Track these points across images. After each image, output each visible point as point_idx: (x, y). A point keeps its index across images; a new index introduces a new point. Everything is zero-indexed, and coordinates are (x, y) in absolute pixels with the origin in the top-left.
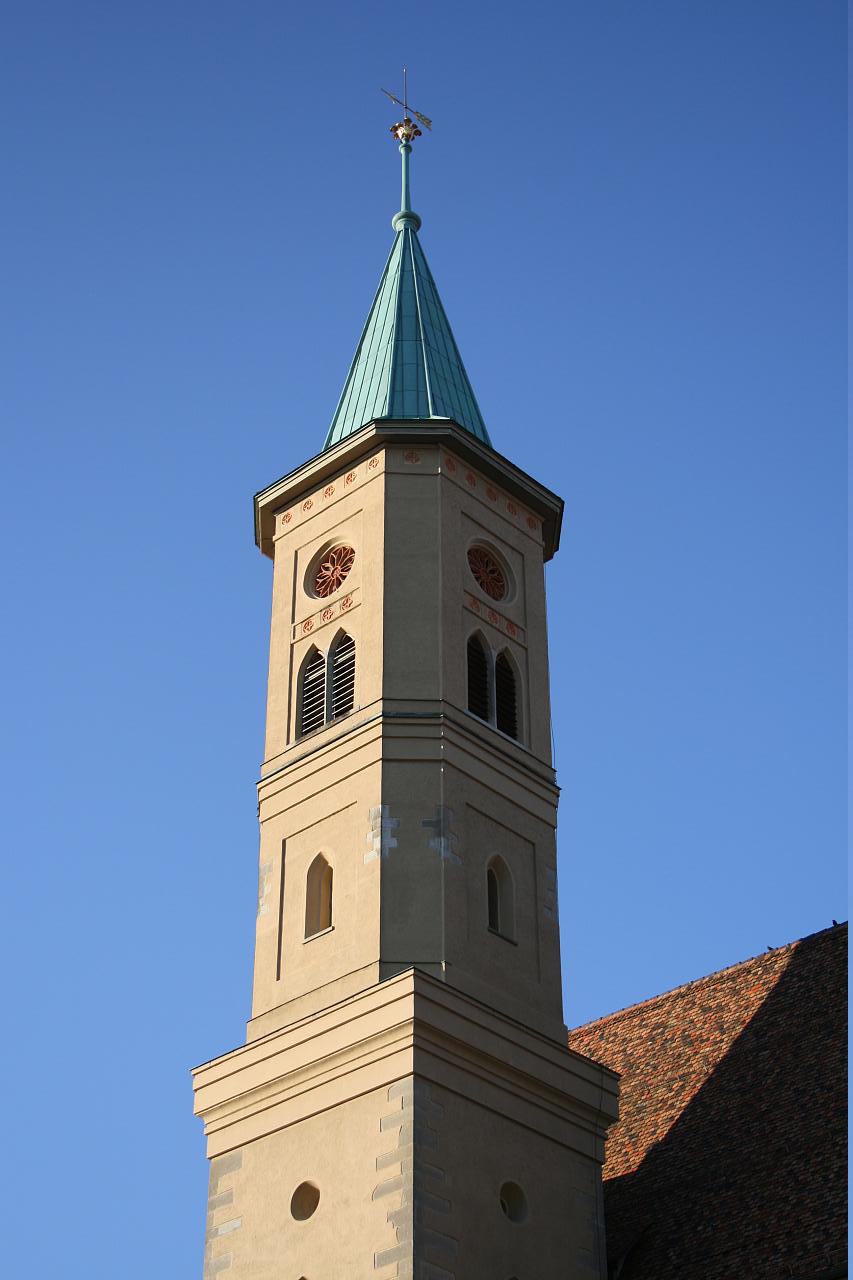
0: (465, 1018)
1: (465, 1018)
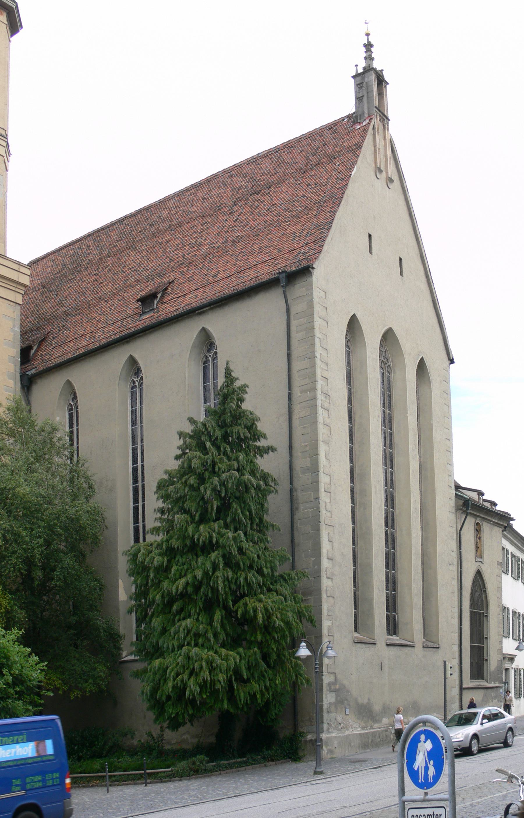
0: (289, 356)
1: (289, 356)
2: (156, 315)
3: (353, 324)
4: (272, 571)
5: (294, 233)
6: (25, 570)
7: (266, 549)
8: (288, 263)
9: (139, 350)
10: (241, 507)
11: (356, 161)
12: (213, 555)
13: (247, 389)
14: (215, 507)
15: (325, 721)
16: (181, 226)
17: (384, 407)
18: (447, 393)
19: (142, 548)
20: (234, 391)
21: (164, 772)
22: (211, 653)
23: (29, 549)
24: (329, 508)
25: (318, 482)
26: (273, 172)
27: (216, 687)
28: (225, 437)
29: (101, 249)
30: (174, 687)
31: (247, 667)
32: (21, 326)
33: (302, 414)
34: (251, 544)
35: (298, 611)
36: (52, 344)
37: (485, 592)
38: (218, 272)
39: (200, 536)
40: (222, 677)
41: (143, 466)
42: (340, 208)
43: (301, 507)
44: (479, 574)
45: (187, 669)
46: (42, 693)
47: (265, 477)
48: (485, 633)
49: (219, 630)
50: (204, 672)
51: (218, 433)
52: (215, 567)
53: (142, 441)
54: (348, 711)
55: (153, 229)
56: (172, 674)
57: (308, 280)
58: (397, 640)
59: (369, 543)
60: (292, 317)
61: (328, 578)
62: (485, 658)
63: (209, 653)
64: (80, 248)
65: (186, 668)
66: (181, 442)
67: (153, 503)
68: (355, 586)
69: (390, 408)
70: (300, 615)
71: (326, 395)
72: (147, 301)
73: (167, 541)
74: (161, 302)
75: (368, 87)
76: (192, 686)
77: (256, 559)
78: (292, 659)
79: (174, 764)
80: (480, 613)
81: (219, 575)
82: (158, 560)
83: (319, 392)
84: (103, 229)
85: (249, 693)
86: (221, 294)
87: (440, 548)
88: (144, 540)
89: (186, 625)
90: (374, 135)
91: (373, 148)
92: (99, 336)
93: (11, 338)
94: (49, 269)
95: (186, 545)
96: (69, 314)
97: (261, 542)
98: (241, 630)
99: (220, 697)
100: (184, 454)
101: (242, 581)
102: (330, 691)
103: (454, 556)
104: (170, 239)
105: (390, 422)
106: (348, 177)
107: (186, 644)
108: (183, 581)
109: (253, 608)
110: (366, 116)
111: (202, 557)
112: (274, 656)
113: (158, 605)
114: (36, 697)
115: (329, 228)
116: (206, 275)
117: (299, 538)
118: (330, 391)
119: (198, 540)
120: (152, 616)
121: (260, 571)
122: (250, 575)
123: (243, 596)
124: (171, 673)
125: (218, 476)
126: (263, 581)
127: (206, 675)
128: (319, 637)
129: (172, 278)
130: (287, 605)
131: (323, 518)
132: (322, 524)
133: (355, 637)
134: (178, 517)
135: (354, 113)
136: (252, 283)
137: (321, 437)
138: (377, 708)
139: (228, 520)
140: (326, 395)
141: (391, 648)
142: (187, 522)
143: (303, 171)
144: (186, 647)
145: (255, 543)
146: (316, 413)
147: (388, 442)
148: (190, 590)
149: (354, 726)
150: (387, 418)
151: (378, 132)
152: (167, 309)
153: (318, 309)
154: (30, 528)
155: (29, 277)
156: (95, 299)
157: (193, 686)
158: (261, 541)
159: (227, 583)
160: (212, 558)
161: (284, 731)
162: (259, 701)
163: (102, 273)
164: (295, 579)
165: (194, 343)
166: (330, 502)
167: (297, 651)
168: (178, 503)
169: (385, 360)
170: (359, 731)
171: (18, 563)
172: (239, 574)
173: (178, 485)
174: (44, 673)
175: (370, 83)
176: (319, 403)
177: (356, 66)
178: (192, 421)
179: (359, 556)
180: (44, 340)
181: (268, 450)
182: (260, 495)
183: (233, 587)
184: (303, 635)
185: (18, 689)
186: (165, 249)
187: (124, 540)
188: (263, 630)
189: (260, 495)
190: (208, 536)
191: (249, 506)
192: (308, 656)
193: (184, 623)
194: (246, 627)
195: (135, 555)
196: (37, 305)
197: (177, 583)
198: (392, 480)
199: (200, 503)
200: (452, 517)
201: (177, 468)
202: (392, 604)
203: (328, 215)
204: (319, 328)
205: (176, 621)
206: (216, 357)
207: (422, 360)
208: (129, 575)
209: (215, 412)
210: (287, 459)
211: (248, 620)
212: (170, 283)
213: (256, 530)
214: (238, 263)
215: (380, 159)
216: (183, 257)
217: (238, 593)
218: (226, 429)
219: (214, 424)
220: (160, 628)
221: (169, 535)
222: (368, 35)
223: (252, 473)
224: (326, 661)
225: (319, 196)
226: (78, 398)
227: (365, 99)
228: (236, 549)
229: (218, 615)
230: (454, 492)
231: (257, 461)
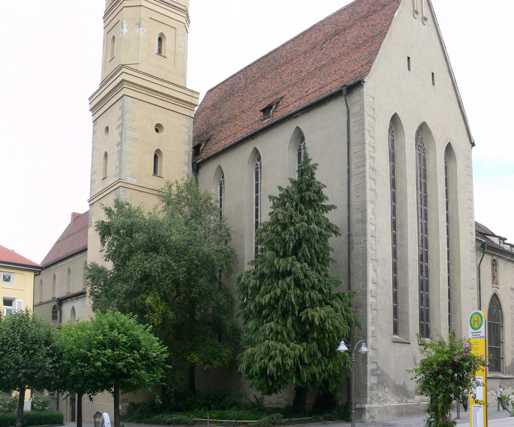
0: (349, 143)
1: (349, 143)
3: (395, 120)
4: (330, 291)
5: (356, 59)
7: (326, 275)
8: (349, 80)
10: (308, 246)
12: (288, 279)
13: (317, 166)
14: (291, 246)
15: (368, 395)
18: (469, 167)
21: (253, 422)
22: (284, 345)
24: (374, 248)
25: (366, 229)
28: (302, 200)
33: (356, 183)
34: (314, 272)
37: (501, 309)
38: (309, 89)
40: (290, 362)
42: (385, 40)
43: (355, 247)
44: (495, 296)
45: (268, 355)
48: (501, 338)
51: (296, 197)
57: (361, 90)
59: (406, 272)
60: (351, 117)
61: (372, 296)
62: (501, 357)
63: (283, 345)
64: (235, 80)
66: (271, 204)
69: (425, 178)
71: (373, 169)
72: (266, 111)
74: (275, 111)
79: (260, 419)
80: (497, 324)
82: (253, 282)
83: (367, 167)
84: (249, 66)
85: (310, 373)
87: (463, 277)
93: (187, 139)
98: (304, 331)
103: (475, 282)
104: (285, 70)
105: (425, 188)
109: (312, 315)
117: (353, 269)
118: (376, 167)
119: (279, 268)
121: (321, 291)
122: (312, 294)
127: (279, 359)
129: (283, 95)
132: (369, 259)
137: (368, 198)
140: (373, 169)
148: (272, 302)
149: (392, 400)
152: (277, 115)
159: (296, 297)
161: (342, 402)
162: (318, 379)
170: (396, 404)
176: (367, 175)
178: (280, 188)
183: (301, 301)
188: (320, 331)
193: (268, 325)
196: (208, 118)
197: (264, 297)
200: (473, 255)
203: (377, 45)
204: (368, 123)
215: (417, 3)
218: (305, 193)
220: (254, 328)
223: (318, 224)
229: (290, 321)
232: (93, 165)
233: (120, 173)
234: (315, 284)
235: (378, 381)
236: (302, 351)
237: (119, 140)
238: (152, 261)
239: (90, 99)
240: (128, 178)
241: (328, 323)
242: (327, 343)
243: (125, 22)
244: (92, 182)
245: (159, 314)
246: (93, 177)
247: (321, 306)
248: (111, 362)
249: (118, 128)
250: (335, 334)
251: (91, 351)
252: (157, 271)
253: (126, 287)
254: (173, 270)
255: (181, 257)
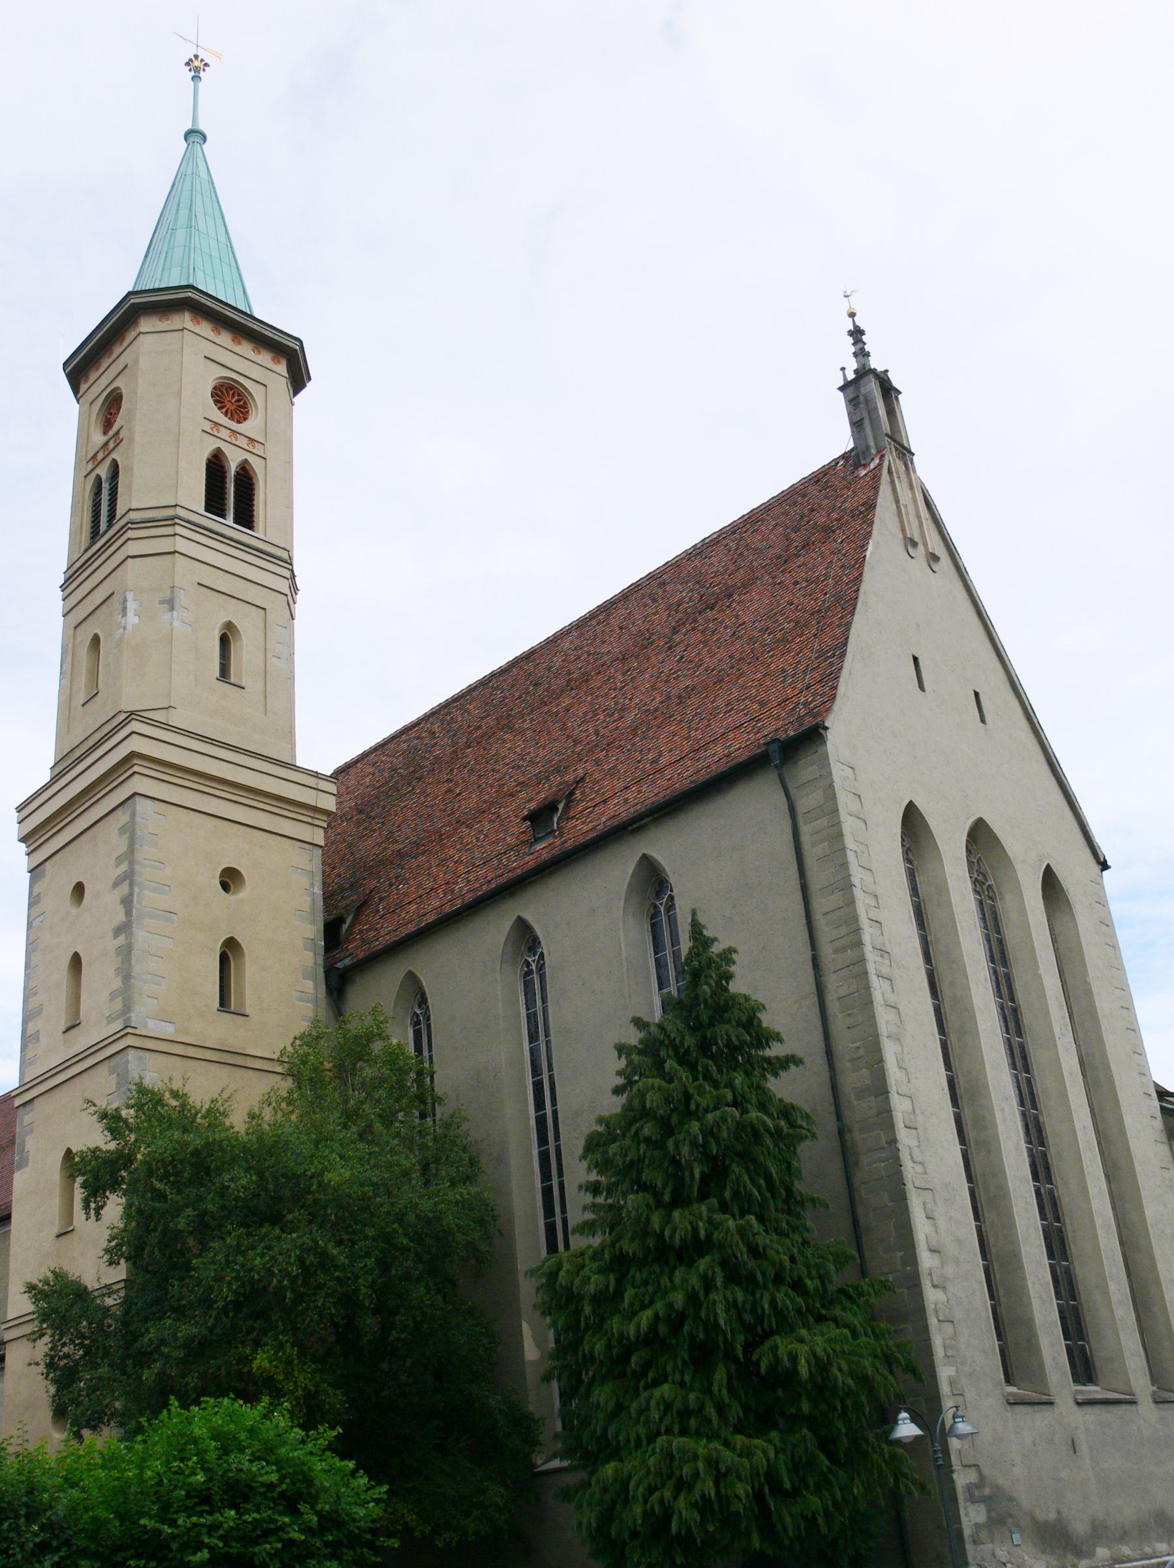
0: (804, 888)
1: (804, 888)
2: (558, 842)
3: (913, 823)
4: (823, 1283)
5: (784, 670)
6: (343, 1318)
7: (805, 1243)
9: (535, 908)
10: (748, 1170)
11: (870, 532)
12: (703, 1264)
15: (970, 1560)
16: (587, 680)
17: (993, 962)
18: (1106, 923)
19: (565, 1260)
20: (710, 961)
22: (715, 1444)
23: (349, 1278)
26: (732, 567)
27: (732, 1509)
28: (704, 1046)
29: (455, 735)
30: (645, 1514)
31: (790, 1465)
32: (324, 883)
33: (843, 992)
34: (775, 1237)
35: (885, 1355)
36: (378, 911)
39: (674, 1229)
40: (741, 1489)
41: (555, 1113)
42: (856, 617)
43: (865, 1160)
45: (669, 1477)
46: (378, 1543)
47: (787, 1112)
49: (727, 1400)
50: (704, 1481)
51: (690, 1041)
52: (708, 1284)
53: (550, 1068)
54: (1017, 1538)
55: (540, 690)
56: (641, 1489)
57: (820, 750)
58: (1096, 1391)
61: (935, 1286)
64: (418, 738)
65: (665, 1477)
67: (577, 1171)
68: (992, 1297)
70: (889, 1360)
71: (883, 952)
72: (540, 818)
73: (613, 1244)
74: (566, 816)
75: (868, 401)
76: (684, 1513)
77: (787, 1263)
78: (884, 1446)
81: (716, 1298)
82: (595, 1283)
83: (868, 949)
86: (668, 791)
88: (567, 1246)
89: (662, 1396)
90: (892, 483)
91: (894, 506)
92: (461, 889)
93: (307, 907)
94: (367, 779)
95: (648, 1249)
96: (407, 855)
97: (793, 1232)
98: (769, 1398)
99: (743, 1526)
100: (630, 1083)
101: (766, 1306)
102: (973, 1500)
104: (571, 706)
105: (1010, 988)
106: (860, 562)
107: (663, 1429)
108: (649, 1313)
109: (790, 1354)
110: (874, 451)
111: (682, 1268)
112: (844, 1443)
113: (602, 1362)
114: (365, 1550)
115: (843, 655)
116: (639, 762)
118: (887, 944)
119: (672, 1237)
120: (592, 1381)
121: (797, 1286)
122: (780, 1296)
123: (768, 1335)
124: (637, 1487)
125: (699, 1119)
126: (807, 1304)
127: (707, 1486)
128: (934, 1399)
129: (581, 772)
130: (858, 1345)
131: (910, 1176)
132: (909, 1187)
133: (1009, 1394)
134: (633, 1201)
135: (853, 450)
136: (723, 767)
138: (1079, 1527)
139: (728, 1194)
140: (883, 952)
141: (1088, 1409)
142: (648, 1206)
143: (784, 561)
144: (664, 1437)
145: (781, 1233)
146: (868, 988)
147: (1012, 1025)
148: (662, 1329)
150: (1017, 1051)
151: (899, 478)
152: (580, 827)
153: (844, 800)
154: (350, 1240)
155: (334, 798)
156: (450, 824)
157: (684, 1510)
158: (795, 1229)
160: (701, 1268)
163: (459, 777)
164: (869, 1294)
165: (630, 884)
166: (918, 1147)
167: (892, 1429)
168: (629, 1174)
169: (981, 878)
171: (328, 1305)
172: (758, 1295)
173: (628, 1141)
174: (382, 1505)
175: (870, 395)
176: (871, 968)
177: (843, 369)
178: (639, 1023)
179: (992, 1240)
180: (364, 904)
181: (787, 1062)
182: (782, 1146)
183: (748, 1318)
184: (900, 1398)
185: (330, 1538)
186: (564, 724)
187: (528, 1246)
189: (782, 1146)
190: (689, 1228)
191: (766, 1167)
192: (917, 1437)
193: (657, 1393)
194: (780, 1393)
195: (553, 1275)
197: (636, 1319)
198: (1032, 1094)
199: (670, 1170)
201: (619, 1110)
202: (1074, 1324)
203: (838, 631)
205: (641, 1389)
206: (673, 905)
207: (1048, 867)
208: (543, 1313)
209: (680, 1003)
210: (825, 1076)
211: (783, 1378)
212: (578, 783)
213: (783, 1211)
214: (693, 733)
215: (909, 522)
216: (597, 733)
217: (759, 1329)
219: (681, 1026)
220: (611, 1405)
221: (614, 1234)
222: (852, 315)
223: (762, 1107)
224: (954, 1444)
225: (816, 600)
226: (429, 1000)
227: (867, 423)
228: (745, 1250)
229: (720, 1375)
230: (1157, 1103)
231: (768, 1085)
232: (29, 993)
233: (127, 1009)
234: (784, 1269)
235: (989, 1518)
236: (772, 1455)
237: (121, 917)
238: (269, 1248)
239: (20, 809)
240: (151, 1023)
241: (840, 1369)
242: (839, 1424)
243: (130, 596)
244: (27, 1039)
245: (297, 1398)
246: (30, 1025)
247: (805, 1325)
248: (236, 1548)
249: (116, 885)
250: (863, 1399)
251: (173, 1523)
252: (289, 1273)
253: (186, 1330)
254: (336, 1267)
255: (354, 1232)
